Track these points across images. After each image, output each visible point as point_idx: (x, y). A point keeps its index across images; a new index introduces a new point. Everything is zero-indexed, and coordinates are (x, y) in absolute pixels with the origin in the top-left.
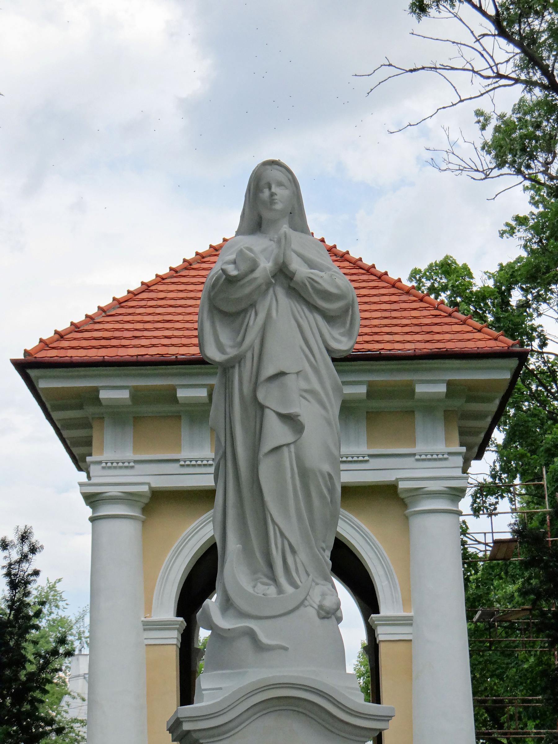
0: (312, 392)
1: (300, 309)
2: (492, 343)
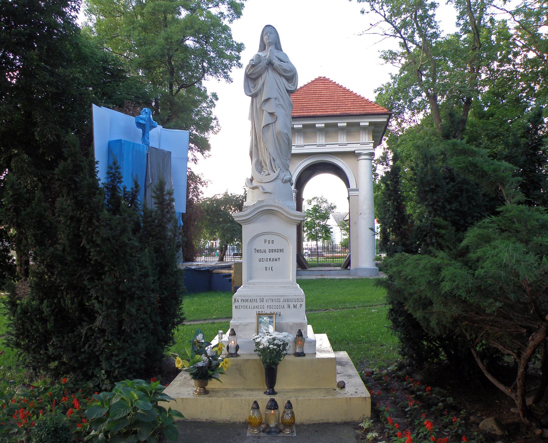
0: (280, 105)
1: (281, 80)
2: (382, 111)
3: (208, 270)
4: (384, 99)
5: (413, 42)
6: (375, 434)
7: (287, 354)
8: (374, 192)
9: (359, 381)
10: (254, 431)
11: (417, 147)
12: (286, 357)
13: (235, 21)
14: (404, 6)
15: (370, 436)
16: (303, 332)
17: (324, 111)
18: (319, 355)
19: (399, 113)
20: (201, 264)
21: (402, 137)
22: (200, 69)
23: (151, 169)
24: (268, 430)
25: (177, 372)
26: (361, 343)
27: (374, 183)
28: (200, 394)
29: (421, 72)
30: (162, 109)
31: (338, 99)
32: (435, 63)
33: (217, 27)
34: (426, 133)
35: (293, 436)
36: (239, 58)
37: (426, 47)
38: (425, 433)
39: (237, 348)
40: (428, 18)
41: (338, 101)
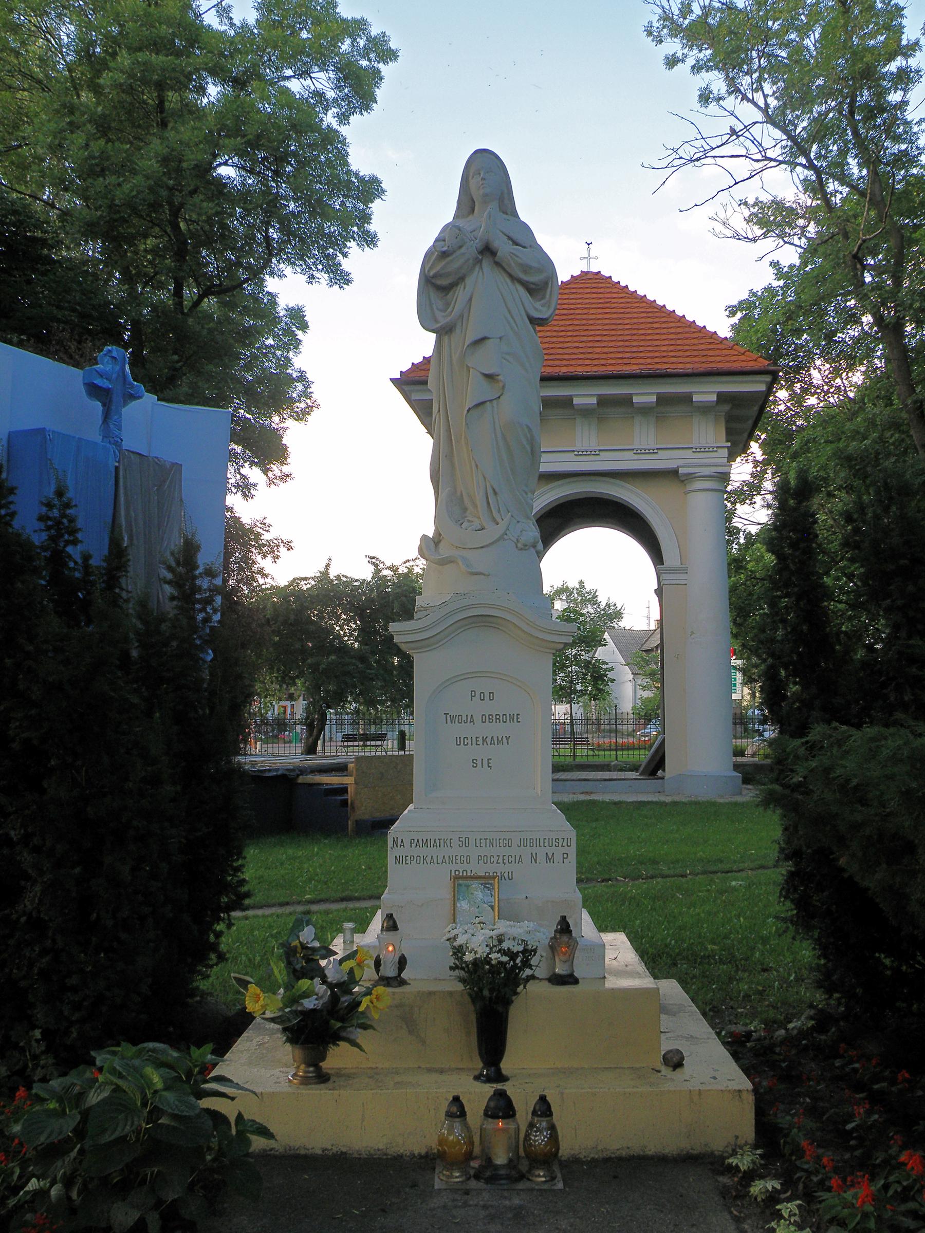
2: (752, 364)
3: (284, 776)
4: (757, 331)
5: (843, 179)
6: (772, 1184)
7: (532, 977)
8: (730, 577)
9: (721, 1053)
10: (451, 1176)
11: (847, 460)
12: (531, 986)
13: (355, 119)
14: (820, 82)
15: (758, 1188)
16: (570, 922)
17: (595, 362)
18: (612, 983)
19: (798, 369)
20: (262, 762)
21: (805, 433)
22: (259, 245)
23: (127, 509)
24: (488, 1174)
25: (243, 1020)
26: (709, 964)
27: (728, 552)
28: (305, 1081)
29: (861, 261)
30: (153, 351)
31: (635, 332)
32: (902, 236)
33: (306, 133)
34: (872, 423)
35: (556, 1188)
36: (366, 218)
37: (877, 192)
38: (905, 1183)
39: (402, 962)
40: (888, 111)
41: (635, 337)
